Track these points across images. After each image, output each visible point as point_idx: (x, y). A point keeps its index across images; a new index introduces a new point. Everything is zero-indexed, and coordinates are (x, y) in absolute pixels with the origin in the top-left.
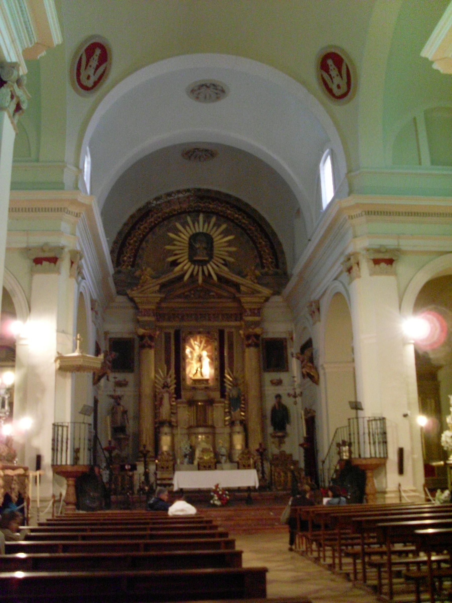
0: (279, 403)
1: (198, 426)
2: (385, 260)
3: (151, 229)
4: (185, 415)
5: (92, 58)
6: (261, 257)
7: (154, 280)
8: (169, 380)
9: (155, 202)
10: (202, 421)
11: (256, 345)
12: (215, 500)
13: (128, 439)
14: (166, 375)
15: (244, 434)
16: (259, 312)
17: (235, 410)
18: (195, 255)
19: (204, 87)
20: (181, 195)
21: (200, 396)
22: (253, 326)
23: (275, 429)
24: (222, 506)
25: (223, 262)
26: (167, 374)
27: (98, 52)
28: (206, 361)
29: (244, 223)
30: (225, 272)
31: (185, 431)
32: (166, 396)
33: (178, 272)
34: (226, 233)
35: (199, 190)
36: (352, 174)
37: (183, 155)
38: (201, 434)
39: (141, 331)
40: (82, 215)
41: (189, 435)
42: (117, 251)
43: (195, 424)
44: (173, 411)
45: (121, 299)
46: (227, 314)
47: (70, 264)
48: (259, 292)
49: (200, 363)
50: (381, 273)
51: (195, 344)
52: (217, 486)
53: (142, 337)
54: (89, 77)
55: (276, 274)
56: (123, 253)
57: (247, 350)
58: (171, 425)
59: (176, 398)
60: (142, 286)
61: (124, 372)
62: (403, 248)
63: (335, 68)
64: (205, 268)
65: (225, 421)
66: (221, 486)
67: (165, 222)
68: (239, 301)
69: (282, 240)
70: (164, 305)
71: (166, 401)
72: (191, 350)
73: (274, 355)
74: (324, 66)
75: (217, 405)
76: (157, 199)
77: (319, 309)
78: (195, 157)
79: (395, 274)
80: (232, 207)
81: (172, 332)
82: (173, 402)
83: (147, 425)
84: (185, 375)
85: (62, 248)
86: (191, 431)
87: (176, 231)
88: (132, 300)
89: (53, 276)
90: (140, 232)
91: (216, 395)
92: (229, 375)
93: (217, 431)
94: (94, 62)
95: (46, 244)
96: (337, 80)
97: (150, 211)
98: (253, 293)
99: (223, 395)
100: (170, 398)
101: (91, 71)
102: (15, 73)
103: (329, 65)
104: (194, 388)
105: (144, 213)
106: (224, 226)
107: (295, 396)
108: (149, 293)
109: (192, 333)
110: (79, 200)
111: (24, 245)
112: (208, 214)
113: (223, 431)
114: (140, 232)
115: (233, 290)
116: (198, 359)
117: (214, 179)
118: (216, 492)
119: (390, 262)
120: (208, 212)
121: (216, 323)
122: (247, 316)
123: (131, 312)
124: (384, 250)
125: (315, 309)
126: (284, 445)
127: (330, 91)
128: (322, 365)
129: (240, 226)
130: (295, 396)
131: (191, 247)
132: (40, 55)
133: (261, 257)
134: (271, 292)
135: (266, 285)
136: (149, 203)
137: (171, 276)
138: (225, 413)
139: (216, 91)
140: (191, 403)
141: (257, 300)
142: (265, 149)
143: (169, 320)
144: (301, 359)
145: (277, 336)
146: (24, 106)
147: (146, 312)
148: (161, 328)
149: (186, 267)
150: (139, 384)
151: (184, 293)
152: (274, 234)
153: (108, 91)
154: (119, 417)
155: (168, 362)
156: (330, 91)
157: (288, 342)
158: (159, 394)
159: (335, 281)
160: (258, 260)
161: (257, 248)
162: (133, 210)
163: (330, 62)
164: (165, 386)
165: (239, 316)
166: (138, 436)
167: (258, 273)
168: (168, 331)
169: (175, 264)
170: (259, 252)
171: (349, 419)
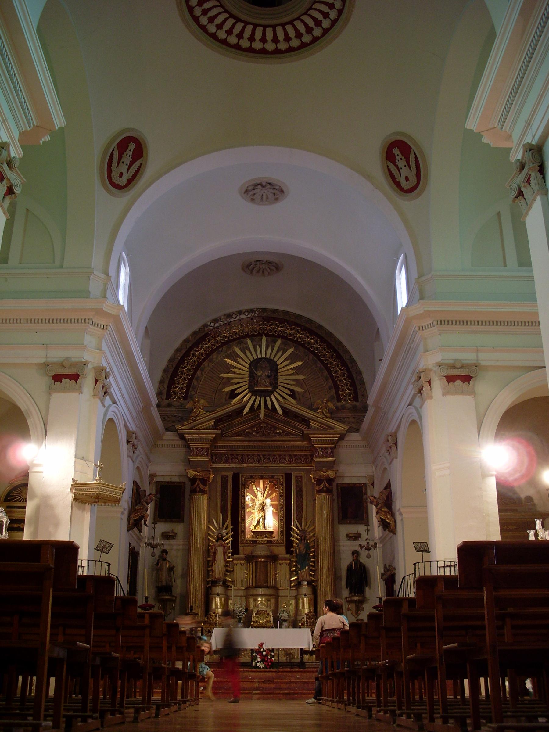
0: (357, 561)
1: (257, 587)
2: (461, 377)
3: (208, 356)
4: (242, 573)
5: (125, 154)
6: (337, 389)
7: (208, 414)
8: (224, 532)
9: (212, 324)
10: (262, 581)
11: (329, 491)
12: (258, 662)
13: (174, 601)
14: (221, 526)
15: (312, 596)
16: (332, 452)
17: (301, 569)
18: (257, 384)
19: (259, 186)
20: (243, 316)
21: (261, 551)
22: (324, 469)
23: (350, 593)
24: (266, 667)
25: (289, 393)
26: (223, 525)
27: (132, 146)
28: (270, 511)
29: (317, 349)
30: (292, 404)
31: (241, 593)
32: (220, 550)
33: (236, 404)
34: (292, 359)
35: (264, 310)
36: (423, 278)
37: (243, 269)
38: (262, 595)
39: (192, 473)
40: (109, 328)
41: (247, 597)
42: (167, 382)
43: (254, 585)
44: (229, 569)
45: (170, 436)
46: (295, 455)
47: (95, 382)
48: (332, 428)
49: (262, 512)
50: (456, 393)
51: (257, 490)
52: (261, 645)
53: (193, 480)
54: (121, 175)
55: (355, 407)
56: (174, 384)
57: (317, 496)
58: (226, 586)
59: (233, 554)
60: (194, 421)
61: (172, 521)
62: (483, 363)
63: (403, 158)
64: (268, 399)
65: (291, 582)
66: (265, 647)
67: (225, 348)
68: (309, 440)
69: (361, 367)
70: (220, 443)
71: (220, 556)
72: (253, 497)
73: (351, 503)
74: (389, 156)
75: (281, 562)
76: (215, 321)
77: (396, 444)
78: (258, 272)
79: (473, 393)
80: (302, 330)
81: (230, 475)
82: (229, 558)
83: (197, 583)
84: (244, 527)
85: (85, 364)
86: (249, 593)
87: (234, 357)
88: (182, 437)
89: (73, 395)
90: (194, 359)
91: (281, 551)
92: (297, 527)
93: (281, 593)
94: (127, 158)
95: (67, 359)
96: (405, 172)
97: (207, 335)
98: (325, 429)
99: (289, 552)
100: (225, 553)
101: (124, 168)
102: (4, 153)
103: (396, 155)
104: (254, 542)
105: (200, 337)
106: (290, 351)
107: (368, 549)
108: (203, 427)
109: (253, 477)
110: (104, 309)
111: (43, 361)
112: (272, 338)
113: (286, 592)
114: (194, 359)
115: (302, 427)
116: (261, 508)
117: (281, 296)
118: (259, 652)
119: (467, 379)
120: (273, 336)
121: (282, 466)
122: (318, 456)
123: (181, 452)
124: (460, 365)
125: (393, 443)
126: (362, 612)
127: (398, 184)
128: (399, 510)
129: (313, 352)
130: (368, 549)
131: (252, 375)
132: (43, 140)
133: (337, 389)
134: (347, 428)
135: (341, 421)
136: (205, 325)
137: (229, 409)
138: (291, 572)
139: (274, 191)
140: (250, 559)
141: (331, 437)
142: (336, 259)
143: (226, 462)
144: (375, 503)
145: (354, 481)
146: (18, 190)
147: (200, 451)
148: (216, 471)
149: (246, 399)
150: (188, 536)
151: (244, 430)
152: (353, 361)
153: (144, 191)
154: (164, 575)
155: (224, 511)
156: (398, 184)
157: (368, 487)
158: (212, 548)
159: (410, 406)
160: (333, 392)
161: (332, 377)
162: (186, 334)
163: (396, 151)
164: (220, 538)
165: (309, 458)
166: (185, 596)
167: (331, 405)
168: (225, 474)
169: (233, 394)
170: (335, 382)
171: (415, 564)
